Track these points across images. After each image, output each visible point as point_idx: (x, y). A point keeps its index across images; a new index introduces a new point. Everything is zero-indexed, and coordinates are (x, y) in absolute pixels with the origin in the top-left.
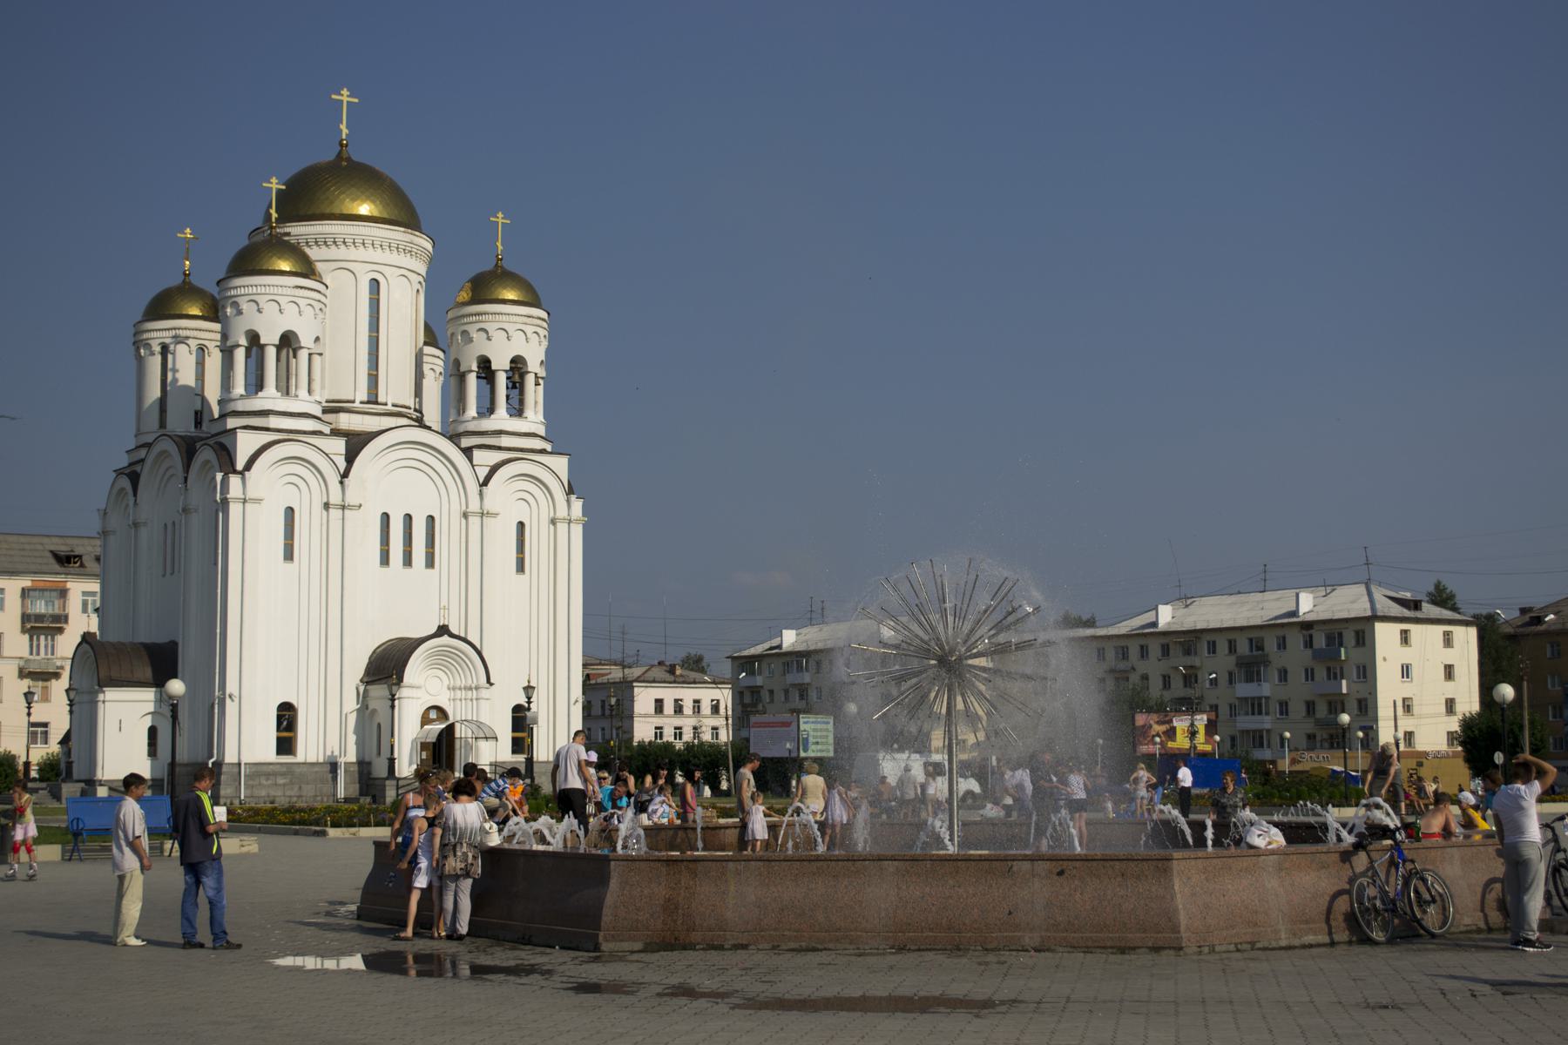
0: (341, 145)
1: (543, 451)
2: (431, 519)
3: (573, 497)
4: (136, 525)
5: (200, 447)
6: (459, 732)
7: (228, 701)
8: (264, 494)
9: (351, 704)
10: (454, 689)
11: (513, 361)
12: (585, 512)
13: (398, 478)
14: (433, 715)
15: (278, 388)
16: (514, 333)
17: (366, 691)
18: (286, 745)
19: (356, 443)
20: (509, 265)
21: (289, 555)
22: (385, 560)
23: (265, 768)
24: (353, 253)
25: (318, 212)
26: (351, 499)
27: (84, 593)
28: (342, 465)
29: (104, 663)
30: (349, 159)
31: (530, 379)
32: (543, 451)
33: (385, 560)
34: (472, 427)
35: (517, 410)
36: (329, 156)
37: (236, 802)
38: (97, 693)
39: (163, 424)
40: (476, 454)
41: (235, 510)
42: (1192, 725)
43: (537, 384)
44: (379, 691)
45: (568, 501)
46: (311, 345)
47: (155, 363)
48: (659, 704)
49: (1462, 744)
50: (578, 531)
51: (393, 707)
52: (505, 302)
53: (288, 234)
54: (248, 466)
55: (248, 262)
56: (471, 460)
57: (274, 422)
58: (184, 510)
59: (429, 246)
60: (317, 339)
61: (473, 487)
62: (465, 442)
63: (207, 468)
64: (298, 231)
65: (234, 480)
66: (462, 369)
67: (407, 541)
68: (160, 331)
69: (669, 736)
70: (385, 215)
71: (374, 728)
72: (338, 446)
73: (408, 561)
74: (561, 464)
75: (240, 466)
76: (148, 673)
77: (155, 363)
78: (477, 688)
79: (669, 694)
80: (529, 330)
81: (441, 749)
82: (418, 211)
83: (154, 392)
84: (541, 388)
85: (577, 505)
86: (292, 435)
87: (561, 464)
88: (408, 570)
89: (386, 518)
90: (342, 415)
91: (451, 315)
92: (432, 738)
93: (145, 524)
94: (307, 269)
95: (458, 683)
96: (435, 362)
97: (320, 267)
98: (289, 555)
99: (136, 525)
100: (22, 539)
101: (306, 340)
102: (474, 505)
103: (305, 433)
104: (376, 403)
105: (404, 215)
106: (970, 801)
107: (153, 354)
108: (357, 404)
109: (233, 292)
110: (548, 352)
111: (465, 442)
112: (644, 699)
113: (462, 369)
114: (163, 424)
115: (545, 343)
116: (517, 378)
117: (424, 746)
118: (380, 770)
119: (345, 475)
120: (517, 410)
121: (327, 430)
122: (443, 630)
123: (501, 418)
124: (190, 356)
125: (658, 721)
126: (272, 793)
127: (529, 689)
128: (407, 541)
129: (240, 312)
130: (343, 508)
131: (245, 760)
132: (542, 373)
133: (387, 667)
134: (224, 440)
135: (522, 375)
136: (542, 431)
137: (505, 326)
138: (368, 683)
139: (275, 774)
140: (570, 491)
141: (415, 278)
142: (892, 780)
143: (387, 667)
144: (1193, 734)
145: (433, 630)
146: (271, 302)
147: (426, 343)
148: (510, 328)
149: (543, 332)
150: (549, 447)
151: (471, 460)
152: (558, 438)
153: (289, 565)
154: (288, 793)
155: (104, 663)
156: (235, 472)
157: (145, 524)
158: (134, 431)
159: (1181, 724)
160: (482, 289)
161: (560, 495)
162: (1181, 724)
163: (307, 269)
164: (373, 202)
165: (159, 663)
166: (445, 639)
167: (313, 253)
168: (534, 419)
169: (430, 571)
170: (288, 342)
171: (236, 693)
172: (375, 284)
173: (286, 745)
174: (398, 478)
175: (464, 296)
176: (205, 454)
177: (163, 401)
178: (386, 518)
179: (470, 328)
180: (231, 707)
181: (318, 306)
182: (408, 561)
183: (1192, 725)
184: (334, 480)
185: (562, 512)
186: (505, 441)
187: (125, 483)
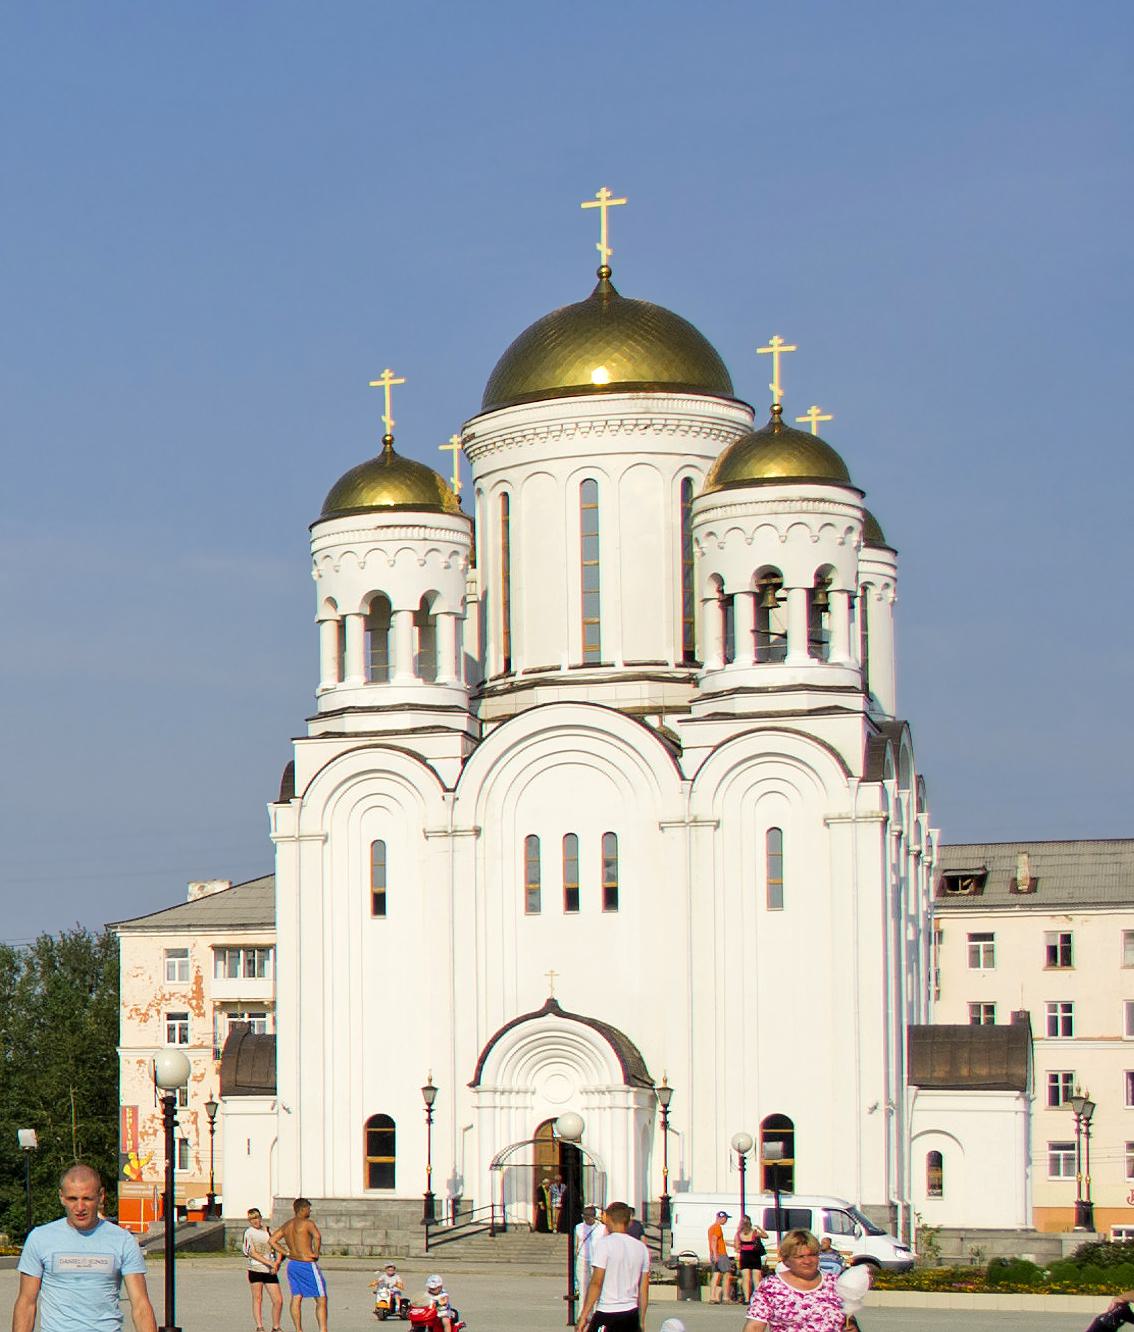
2: (610, 836)
13: (572, 777)
18: (381, 1175)
22: (533, 904)
23: (335, 1206)
24: (551, 447)
27: (974, 937)
33: (533, 904)
49: (743, 1253)
70: (665, 378)
89: (532, 841)
104: (598, 665)
108: (671, 667)
122: (552, 1007)
126: (344, 1240)
139: (349, 1214)
145: (539, 1006)
148: (748, 524)
154: (368, 1241)
166: (551, 1018)
172: (589, 486)
173: (381, 1175)
178: (532, 841)
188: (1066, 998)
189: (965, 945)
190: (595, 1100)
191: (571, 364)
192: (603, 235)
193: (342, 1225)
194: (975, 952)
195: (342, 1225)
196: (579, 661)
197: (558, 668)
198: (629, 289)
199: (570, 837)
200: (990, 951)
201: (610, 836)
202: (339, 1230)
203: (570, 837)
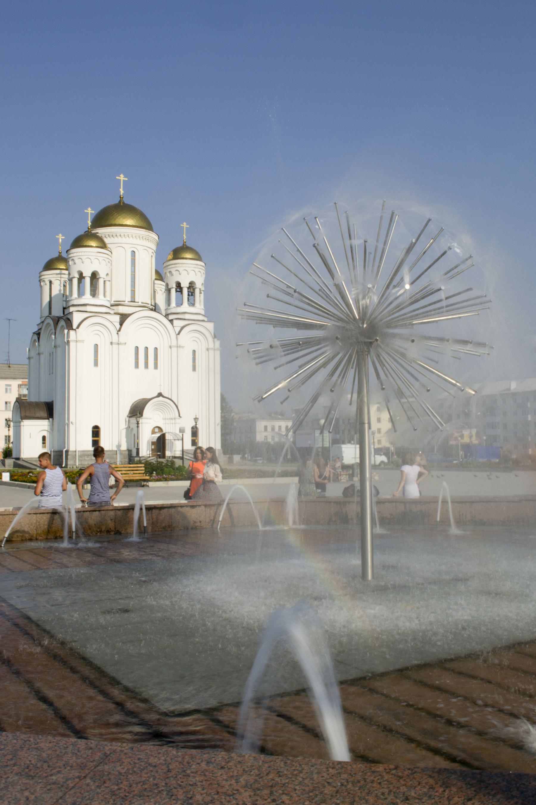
0: (121, 197)
1: (203, 321)
2: (156, 349)
3: (216, 340)
4: (39, 354)
5: (60, 320)
6: (168, 437)
7: (71, 425)
8: (84, 340)
9: (123, 426)
10: (165, 419)
11: (190, 283)
12: (221, 345)
14: (157, 430)
15: (91, 295)
16: (189, 271)
17: (129, 421)
19: (124, 318)
20: (188, 244)
21: (96, 364)
22: (137, 366)
23: (85, 453)
24: (123, 240)
25: (110, 224)
26: (121, 341)
27: (6, 385)
28: (118, 326)
29: (25, 409)
30: (124, 203)
31: (197, 291)
32: (203, 321)
33: (137, 366)
34: (173, 311)
35: (192, 304)
36: (116, 201)
37: (75, 467)
38: (20, 422)
39: (50, 312)
40: (175, 321)
41: (72, 345)
42: (471, 433)
43: (200, 293)
44: (133, 420)
45: (214, 341)
46: (105, 277)
47: (46, 289)
48: (266, 428)
50: (218, 353)
51: (138, 427)
52: (186, 259)
53: (98, 233)
54: (78, 327)
55: (78, 243)
56: (172, 324)
57: (88, 308)
58: (55, 346)
59: (156, 238)
60: (107, 274)
61: (173, 335)
62: (171, 317)
63: (62, 328)
64: (101, 231)
65: (72, 332)
66: (169, 287)
67: (146, 358)
68: (49, 275)
69: (269, 440)
70: (141, 225)
71: (133, 435)
72: (117, 318)
73: (146, 366)
74: (210, 326)
75: (75, 327)
76: (46, 415)
77: (46, 289)
78: (175, 419)
79: (269, 424)
80: (197, 270)
81: (160, 444)
82: (151, 221)
83: (46, 299)
84: (202, 295)
85: (218, 343)
86: (97, 314)
87: (210, 326)
88: (146, 370)
89: (137, 348)
90: (120, 307)
91: (165, 265)
92: (155, 440)
93: (43, 353)
94: (103, 246)
95: (171, 417)
96: (160, 286)
97: (108, 246)
98: (96, 364)
99: (39, 354)
100: (19, 366)
101: (102, 274)
102: (174, 343)
103: (102, 313)
104: (134, 302)
105: (148, 225)
106: (383, 466)
107: (46, 284)
109: (72, 255)
110: (205, 280)
111: (171, 317)
112: (260, 425)
113: (169, 287)
114: (50, 312)
115: (204, 276)
116: (192, 290)
117: (153, 443)
118: (134, 454)
119: (119, 330)
120: (192, 304)
121: (112, 312)
122: (160, 395)
123: (185, 307)
124: (55, 281)
125: (265, 434)
127: (196, 419)
128: (146, 358)
129: (75, 264)
130: (118, 344)
131: (78, 449)
132: (203, 289)
133: (137, 411)
134: (69, 317)
135: (194, 290)
136: (203, 312)
137: (187, 269)
138: (130, 417)
140: (215, 337)
141: (151, 251)
142: (104, 623)
143: (137, 411)
144: (471, 437)
145: (156, 395)
146: (87, 259)
147: (156, 279)
149: (203, 272)
150: (206, 319)
151: (172, 324)
152: (210, 314)
153: (96, 368)
155: (25, 409)
156: (73, 329)
157: (43, 353)
158: (40, 316)
159: (466, 433)
160: (177, 254)
161: (210, 339)
162: (466, 433)
163: (103, 246)
164: (132, 219)
165: (48, 410)
166: (161, 398)
167: (106, 240)
168: (199, 307)
169: (156, 370)
170: (94, 276)
171: (74, 422)
174: (144, 331)
175: (171, 257)
176: (62, 323)
177: (50, 302)
178: (137, 348)
179: (172, 270)
180: (72, 427)
181: (107, 260)
182: (146, 366)
183: (471, 433)
184: (114, 332)
185: (211, 345)
186: (187, 316)
187: (36, 337)
188: (4, 403)
189: (4, 387)
190: (167, 421)
191: (117, 217)
192: (122, 186)
193: (89, 458)
194: (6, 389)
195: (89, 458)
196: (130, 300)
197: (125, 301)
198: (127, 201)
199: (147, 348)
200: (11, 389)
201: (156, 349)
202: (88, 460)
203: (147, 348)
